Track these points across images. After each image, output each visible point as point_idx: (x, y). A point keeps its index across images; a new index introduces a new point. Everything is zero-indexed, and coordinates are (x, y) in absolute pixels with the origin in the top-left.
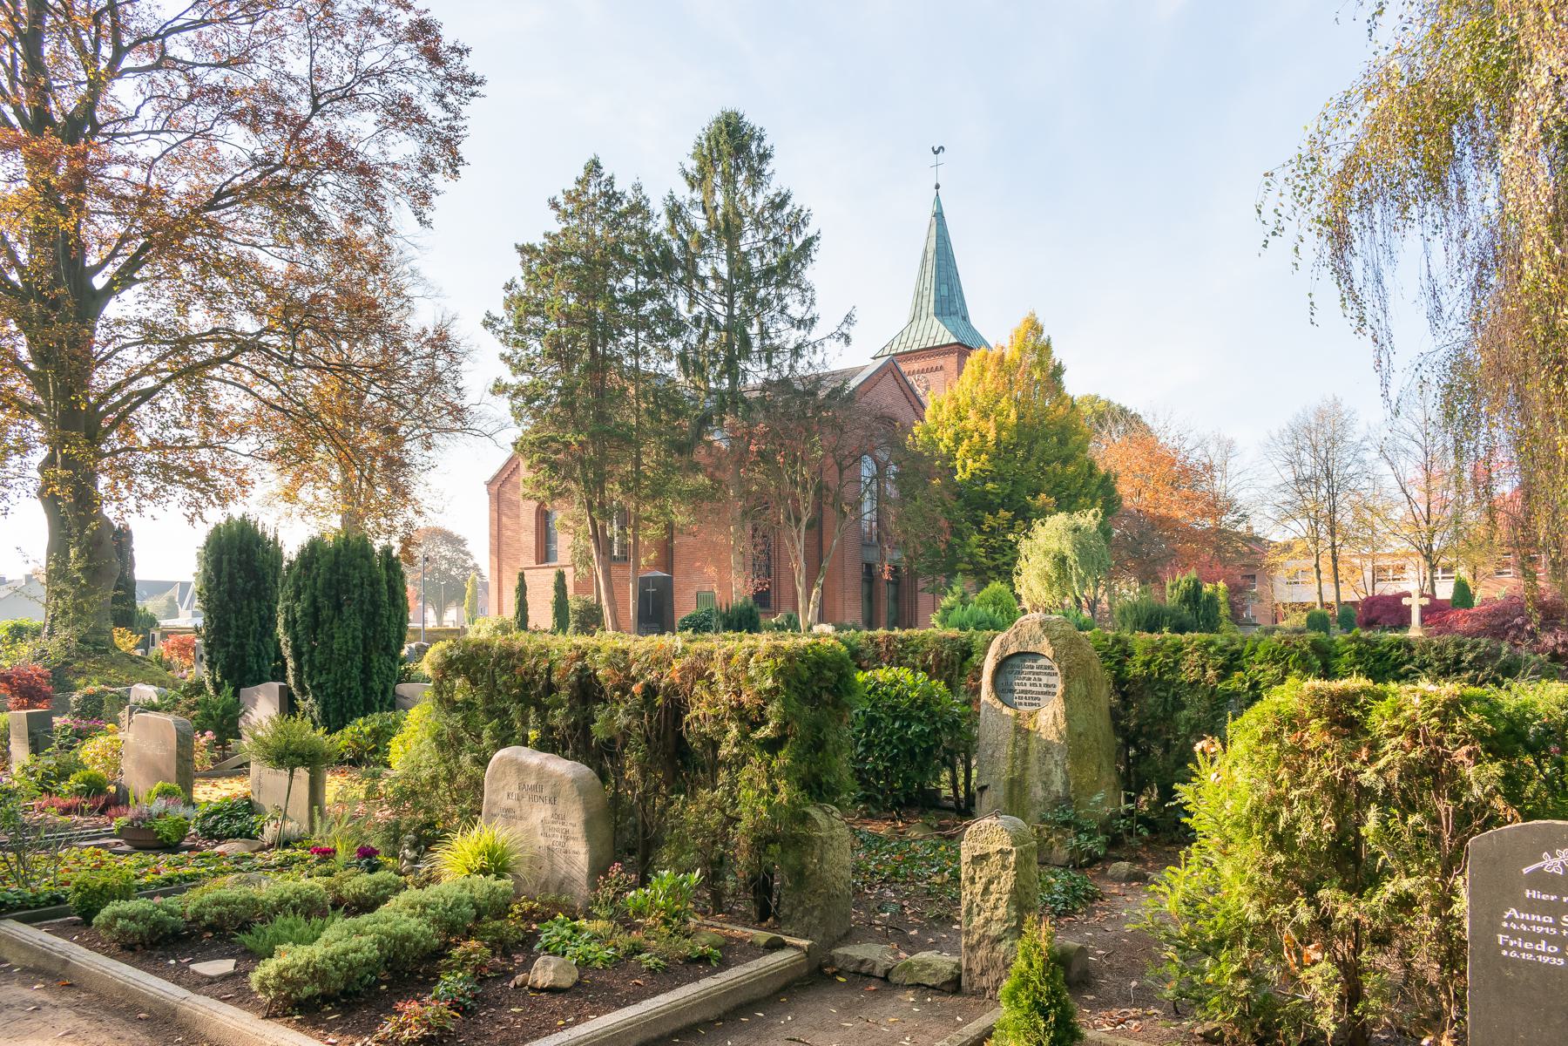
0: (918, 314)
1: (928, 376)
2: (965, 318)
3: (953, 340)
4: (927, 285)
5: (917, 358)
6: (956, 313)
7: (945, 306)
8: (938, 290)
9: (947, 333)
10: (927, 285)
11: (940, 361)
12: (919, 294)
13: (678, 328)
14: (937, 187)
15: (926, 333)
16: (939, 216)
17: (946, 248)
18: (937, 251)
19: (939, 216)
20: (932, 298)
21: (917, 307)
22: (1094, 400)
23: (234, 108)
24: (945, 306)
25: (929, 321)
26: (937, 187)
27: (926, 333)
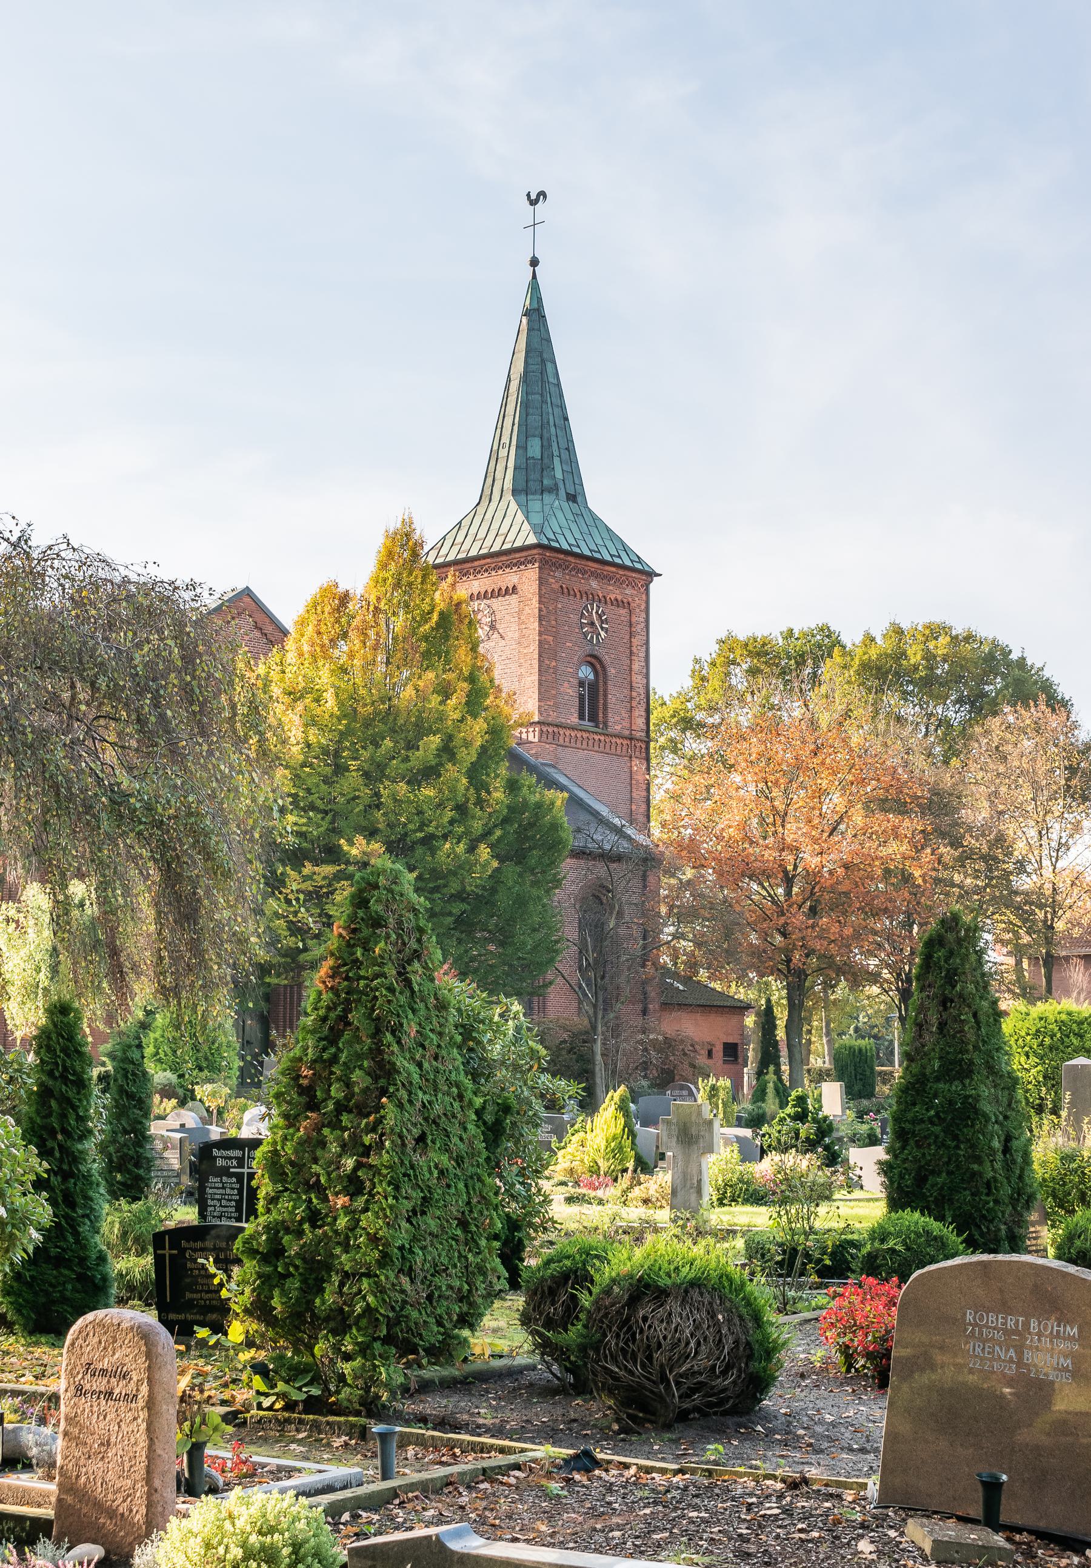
0: (487, 492)
1: (496, 603)
2: (575, 497)
3: (532, 540)
4: (505, 439)
5: (477, 571)
6: (554, 489)
7: (534, 476)
8: (522, 447)
9: (526, 526)
10: (505, 439)
11: (510, 578)
12: (494, 456)
13: (121, 1211)
14: (534, 262)
15: (495, 526)
16: (535, 315)
17: (543, 372)
18: (525, 378)
19: (535, 315)
20: (511, 464)
21: (489, 477)
22: (934, 631)
23: (328, 869)
24: (534, 476)
25: (504, 504)
26: (534, 262)
27: (495, 526)
